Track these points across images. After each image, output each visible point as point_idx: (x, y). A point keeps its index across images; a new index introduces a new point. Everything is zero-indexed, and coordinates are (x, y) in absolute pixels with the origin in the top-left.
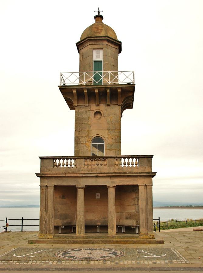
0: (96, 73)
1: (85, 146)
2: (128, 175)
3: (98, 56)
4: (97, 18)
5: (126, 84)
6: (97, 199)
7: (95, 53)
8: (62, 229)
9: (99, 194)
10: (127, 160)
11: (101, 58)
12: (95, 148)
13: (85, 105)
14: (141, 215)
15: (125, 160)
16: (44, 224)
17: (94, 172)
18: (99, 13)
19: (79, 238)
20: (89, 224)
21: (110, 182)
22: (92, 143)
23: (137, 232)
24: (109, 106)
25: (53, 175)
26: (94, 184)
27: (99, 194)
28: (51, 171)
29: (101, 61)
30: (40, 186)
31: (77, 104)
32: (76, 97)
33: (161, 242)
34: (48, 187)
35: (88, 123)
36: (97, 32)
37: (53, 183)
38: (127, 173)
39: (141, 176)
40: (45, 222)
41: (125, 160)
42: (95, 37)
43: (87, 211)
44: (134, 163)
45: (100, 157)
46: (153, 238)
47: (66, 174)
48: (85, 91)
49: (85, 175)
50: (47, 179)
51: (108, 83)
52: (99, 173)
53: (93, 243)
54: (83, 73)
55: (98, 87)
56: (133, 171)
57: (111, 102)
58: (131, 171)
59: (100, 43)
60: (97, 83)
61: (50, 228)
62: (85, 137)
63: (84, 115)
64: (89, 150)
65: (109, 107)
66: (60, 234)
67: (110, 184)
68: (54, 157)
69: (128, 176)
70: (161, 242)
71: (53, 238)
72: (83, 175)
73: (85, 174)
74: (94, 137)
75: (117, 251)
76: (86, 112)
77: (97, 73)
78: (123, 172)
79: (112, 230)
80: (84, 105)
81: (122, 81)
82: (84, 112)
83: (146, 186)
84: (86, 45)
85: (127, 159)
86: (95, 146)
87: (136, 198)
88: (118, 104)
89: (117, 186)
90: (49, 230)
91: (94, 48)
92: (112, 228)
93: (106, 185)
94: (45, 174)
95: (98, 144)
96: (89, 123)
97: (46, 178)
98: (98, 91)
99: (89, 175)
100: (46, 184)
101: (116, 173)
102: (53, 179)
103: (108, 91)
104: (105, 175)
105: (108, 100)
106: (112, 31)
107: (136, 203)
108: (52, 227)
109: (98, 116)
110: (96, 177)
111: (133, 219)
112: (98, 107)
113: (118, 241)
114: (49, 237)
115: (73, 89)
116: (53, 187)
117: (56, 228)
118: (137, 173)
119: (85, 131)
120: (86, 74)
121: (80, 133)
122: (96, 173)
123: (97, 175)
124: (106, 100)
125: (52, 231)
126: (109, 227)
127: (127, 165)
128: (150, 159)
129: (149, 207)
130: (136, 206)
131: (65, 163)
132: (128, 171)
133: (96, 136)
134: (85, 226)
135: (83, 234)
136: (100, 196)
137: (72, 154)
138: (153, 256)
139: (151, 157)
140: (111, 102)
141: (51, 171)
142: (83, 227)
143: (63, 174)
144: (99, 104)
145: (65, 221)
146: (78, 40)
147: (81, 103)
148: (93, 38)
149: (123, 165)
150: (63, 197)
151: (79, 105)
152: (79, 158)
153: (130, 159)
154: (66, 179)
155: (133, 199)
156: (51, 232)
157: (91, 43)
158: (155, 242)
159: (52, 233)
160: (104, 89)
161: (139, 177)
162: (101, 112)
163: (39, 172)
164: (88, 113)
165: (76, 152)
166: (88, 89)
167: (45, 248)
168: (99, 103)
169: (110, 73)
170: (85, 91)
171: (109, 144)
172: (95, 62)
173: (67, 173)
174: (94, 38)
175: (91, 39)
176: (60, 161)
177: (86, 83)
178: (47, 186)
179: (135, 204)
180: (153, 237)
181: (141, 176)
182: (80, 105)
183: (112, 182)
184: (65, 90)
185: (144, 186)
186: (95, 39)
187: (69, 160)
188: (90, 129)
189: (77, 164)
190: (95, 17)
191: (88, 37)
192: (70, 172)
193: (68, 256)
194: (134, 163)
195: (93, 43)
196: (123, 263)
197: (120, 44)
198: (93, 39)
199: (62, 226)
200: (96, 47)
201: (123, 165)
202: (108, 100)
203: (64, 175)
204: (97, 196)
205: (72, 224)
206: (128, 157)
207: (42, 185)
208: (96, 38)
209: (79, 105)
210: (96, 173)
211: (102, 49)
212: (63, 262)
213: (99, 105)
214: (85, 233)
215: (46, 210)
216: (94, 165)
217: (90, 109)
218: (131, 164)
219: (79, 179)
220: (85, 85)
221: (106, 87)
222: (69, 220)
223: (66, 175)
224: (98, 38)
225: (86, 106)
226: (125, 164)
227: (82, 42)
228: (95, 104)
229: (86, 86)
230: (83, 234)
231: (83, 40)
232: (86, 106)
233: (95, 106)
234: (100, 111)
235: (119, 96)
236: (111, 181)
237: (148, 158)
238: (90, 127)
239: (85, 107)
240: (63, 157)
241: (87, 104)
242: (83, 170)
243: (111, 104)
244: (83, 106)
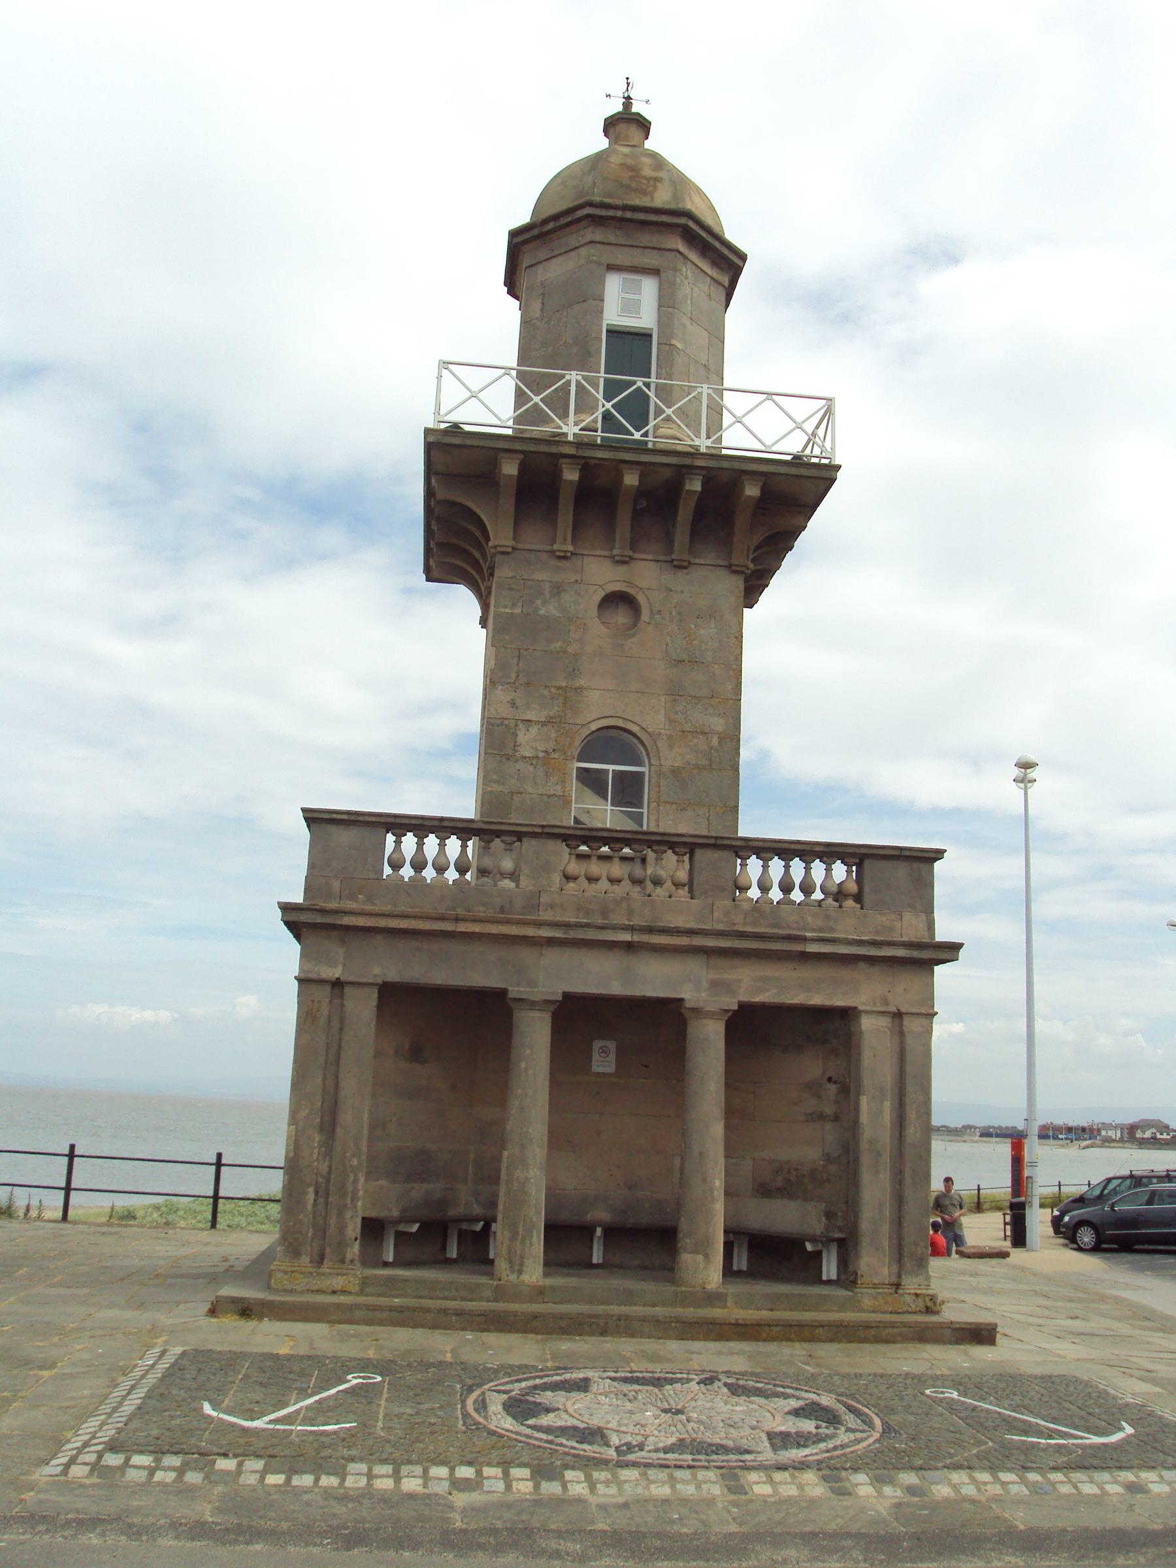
0: (635, 383)
1: (540, 772)
2: (812, 948)
3: (631, 307)
4: (622, 127)
5: (789, 458)
6: (598, 1074)
7: (614, 286)
8: (399, 1235)
9: (612, 1045)
10: (409, 841)
11: (645, 318)
12: (588, 793)
13: (552, 552)
14: (866, 1177)
15: (787, 867)
16: (309, 1207)
17: (620, 919)
18: (628, 100)
19: (516, 1297)
20: (565, 1216)
21: (705, 984)
22: (579, 761)
23: (830, 1269)
24: (685, 568)
25: (382, 923)
26: (616, 988)
27: (612, 1045)
28: (370, 899)
29: (645, 336)
30: (301, 980)
31: (511, 543)
32: (508, 504)
33: (982, 1335)
34: (348, 990)
35: (565, 652)
36: (634, 185)
37: (377, 970)
38: (804, 939)
39: (872, 960)
40: (317, 1193)
41: (787, 867)
42: (625, 208)
43: (558, 1140)
44: (818, 883)
45: (654, 838)
46: (928, 1311)
47: (457, 919)
48: (571, 475)
49: (572, 934)
50: (343, 942)
51: (565, 429)
52: (651, 930)
53: (603, 1333)
54: (563, 376)
55: (645, 458)
56: (832, 930)
57: (691, 550)
58: (821, 930)
59: (646, 238)
60: (637, 436)
61: (342, 1229)
62: (544, 724)
63: (544, 603)
64: (566, 801)
65: (681, 574)
66: (386, 1264)
67: (703, 995)
68: (396, 816)
69: (804, 957)
70: (982, 1335)
71: (362, 1292)
72: (558, 934)
73: (567, 926)
74: (594, 727)
75: (589, 1374)
76: (558, 589)
77: (640, 384)
78: (782, 932)
79: (706, 1256)
80: (548, 548)
81: (767, 443)
82: (547, 587)
83: (898, 1015)
84: (573, 241)
85: (454, 837)
86: (593, 782)
87: (830, 1080)
88: (734, 562)
89: (567, 996)
90: (339, 1244)
91: (612, 261)
92: (703, 1248)
93: (681, 1000)
94: (336, 912)
95: (611, 767)
96: (571, 649)
97: (335, 933)
98: (763, 490)
99: (591, 935)
100: (336, 972)
101: (742, 935)
102: (379, 941)
103: (696, 485)
104: (683, 941)
105: (681, 535)
106: (699, 194)
107: (829, 1110)
108: (354, 1228)
109: (621, 617)
110: (629, 947)
111: (806, 1200)
112: (624, 568)
113: (746, 1325)
114: (338, 1282)
115: (622, 466)
116: (374, 994)
117: (373, 1229)
118: (860, 943)
119: (546, 692)
120: (578, 384)
121: (519, 702)
122: (632, 929)
123: (636, 938)
124: (669, 539)
125: (354, 1250)
126: (685, 1242)
127: (797, 896)
128: (923, 867)
129: (912, 1132)
130: (828, 1126)
131: (797, 880)
132: (805, 929)
133: (621, 723)
134: (547, 1227)
135: (534, 1279)
136: (612, 1057)
137: (465, 807)
138: (1082, 1438)
139: (938, 854)
140: (691, 550)
141: (370, 899)
142: (539, 1237)
143: (442, 918)
144: (630, 553)
145: (419, 1190)
146: (523, 217)
147: (534, 538)
148: (611, 213)
149: (754, 893)
150: (416, 1053)
151: (520, 546)
152: (534, 835)
153: (410, 835)
154: (455, 947)
155: (813, 1088)
156: (349, 1256)
157: (598, 237)
158: (948, 1333)
159: (352, 1261)
160: (668, 473)
161: (862, 965)
162: (641, 598)
163: (298, 898)
164: (567, 598)
165: (487, 800)
166: (588, 468)
167: (360, 1357)
168: (634, 552)
169: (710, 391)
170: (571, 475)
171: (675, 772)
172: (613, 332)
173: (461, 912)
174: (619, 214)
175: (604, 213)
176: (442, 845)
177: (576, 430)
178: (338, 984)
179: (821, 1117)
180: (929, 1304)
181: (872, 960)
182: (529, 547)
183: (714, 984)
184: (286, 908)
185: (328, 988)
186: (622, 219)
187: (432, 841)
188: (577, 685)
189: (525, 869)
190: (611, 125)
191: (590, 204)
192: (480, 911)
193: (563, 1431)
194: (818, 883)
195: (611, 238)
196: (425, 1475)
197: (740, 263)
198: (613, 218)
199: (402, 1220)
200: (622, 257)
201: (387, 870)
202: (681, 535)
203: (449, 927)
204: (596, 1056)
205: (452, 1212)
206: (786, 850)
207: (313, 976)
208: (628, 215)
209: (637, 556)
210: (632, 929)
211: (654, 272)
212: (353, 1467)
213: (632, 558)
214: (547, 1264)
215: (329, 1125)
216: (619, 881)
217: (578, 577)
218: (797, 888)
219: (527, 955)
220: (570, 438)
221: (687, 461)
222: (435, 1188)
223: (462, 927)
224: (641, 216)
225: (559, 558)
226: (764, 887)
227: (551, 226)
228: (606, 553)
229: (579, 444)
230: (534, 1274)
231: (545, 222)
232: (559, 558)
233: (607, 565)
234: (632, 591)
235: (741, 521)
236: (712, 976)
237: (915, 865)
238: (574, 673)
239: (553, 562)
240: (442, 819)
241: (564, 548)
242: (552, 906)
243: (693, 561)
244: (544, 556)
